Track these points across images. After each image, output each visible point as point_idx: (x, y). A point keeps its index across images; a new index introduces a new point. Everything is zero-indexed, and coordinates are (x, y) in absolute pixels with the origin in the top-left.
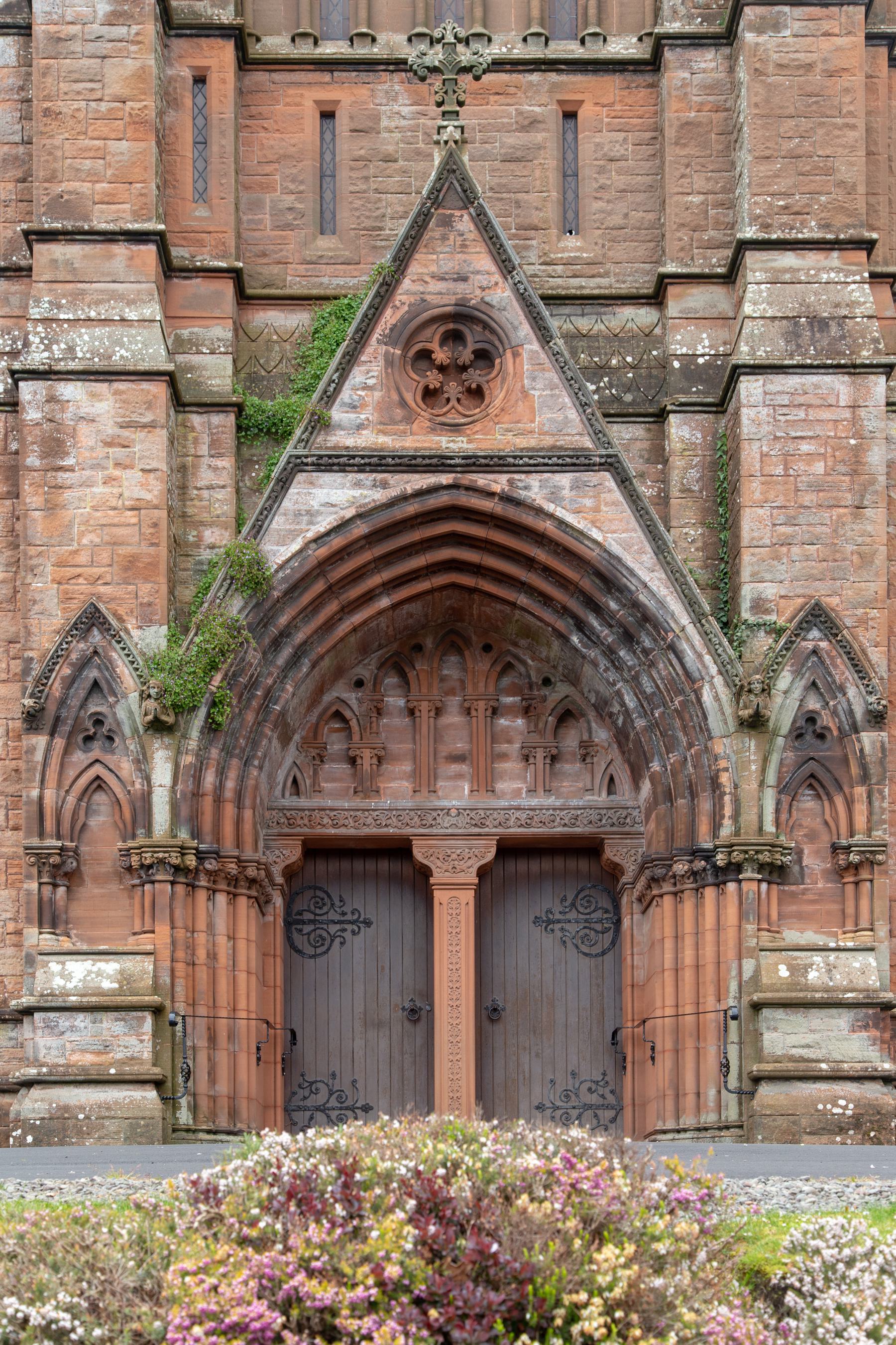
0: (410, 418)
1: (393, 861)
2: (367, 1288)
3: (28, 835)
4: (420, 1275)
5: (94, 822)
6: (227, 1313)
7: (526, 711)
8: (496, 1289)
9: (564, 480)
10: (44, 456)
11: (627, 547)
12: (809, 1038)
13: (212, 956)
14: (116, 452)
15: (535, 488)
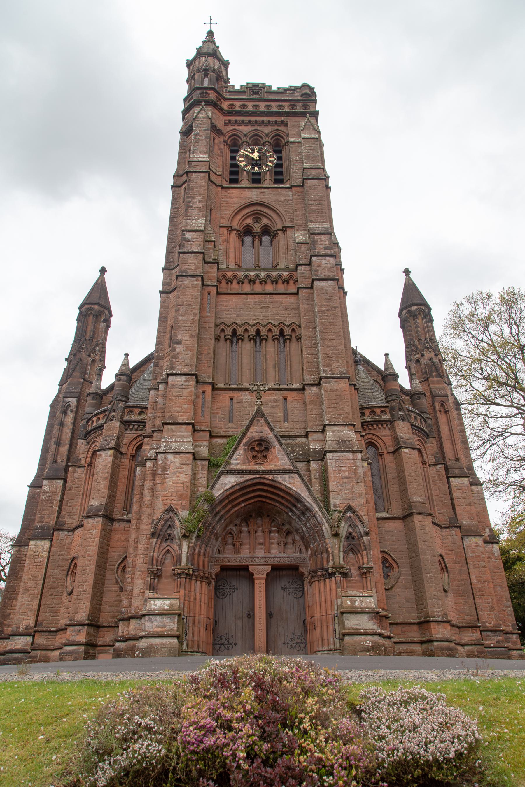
0: (249, 462)
1: (244, 572)
2: (241, 713)
3: (149, 565)
4: (256, 708)
5: (166, 562)
6: (200, 722)
7: (278, 532)
8: (278, 713)
9: (286, 476)
10: (162, 471)
11: (302, 491)
12: (357, 622)
13: (195, 599)
14: (179, 470)
15: (279, 478)
